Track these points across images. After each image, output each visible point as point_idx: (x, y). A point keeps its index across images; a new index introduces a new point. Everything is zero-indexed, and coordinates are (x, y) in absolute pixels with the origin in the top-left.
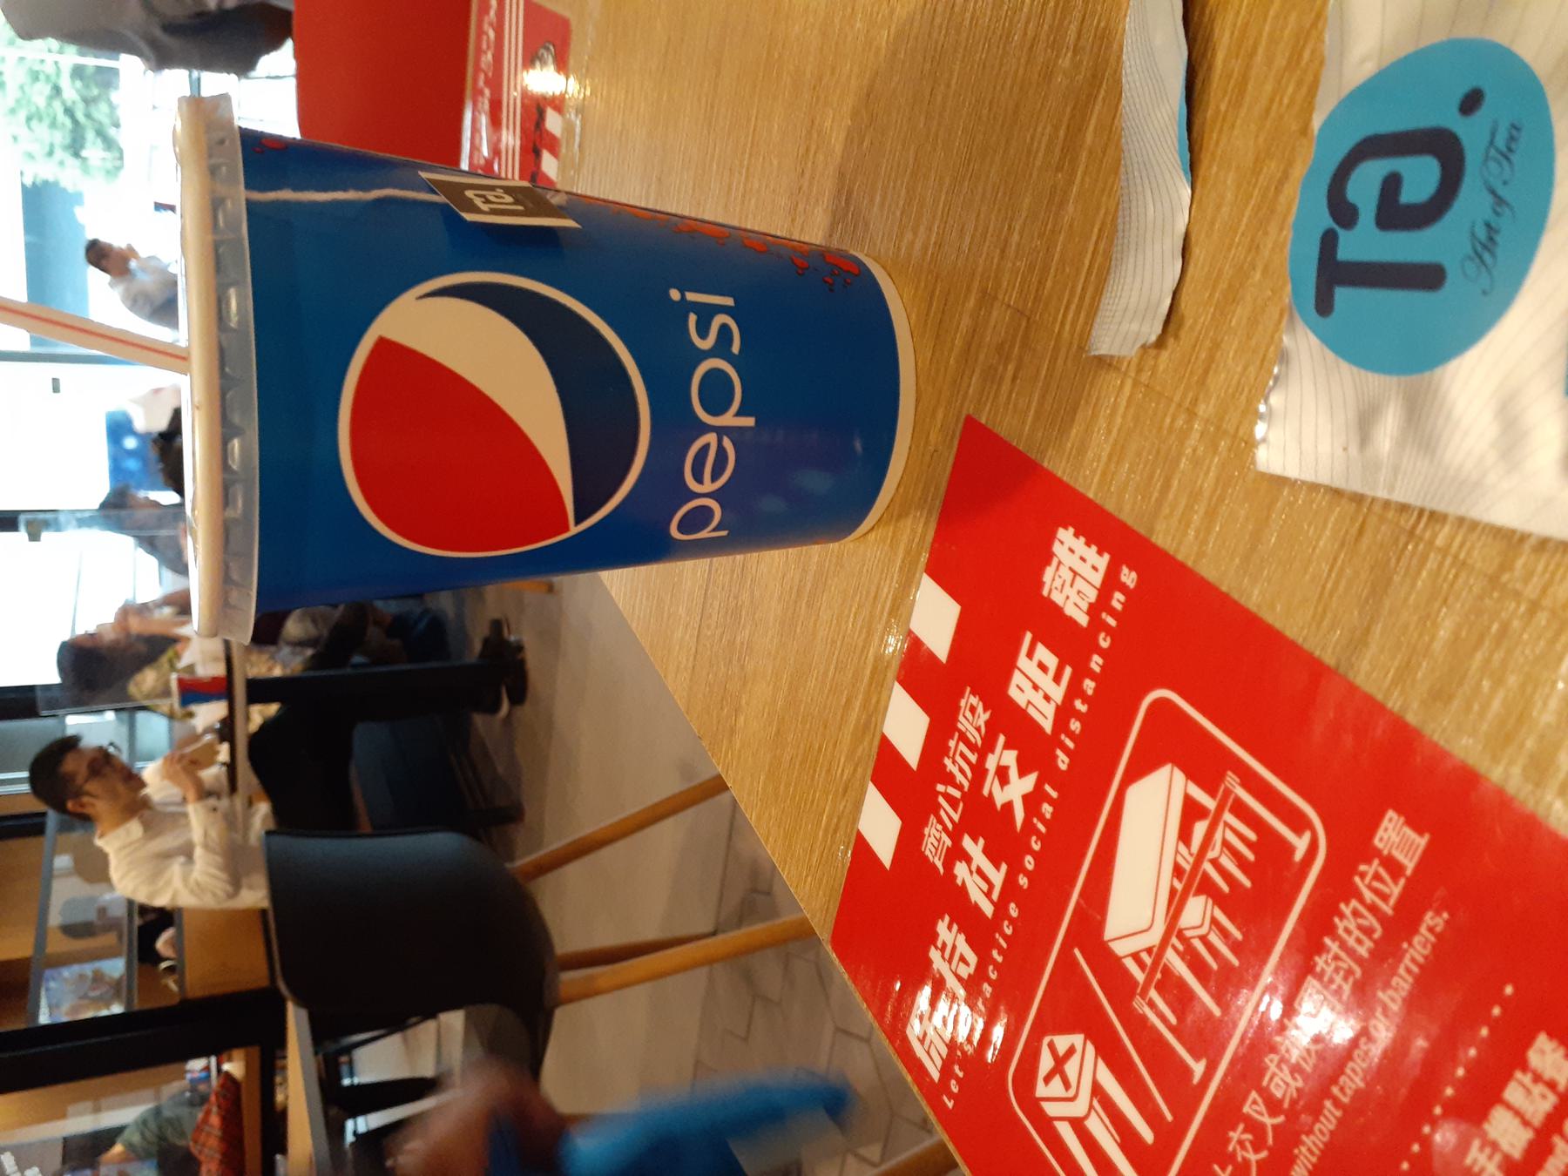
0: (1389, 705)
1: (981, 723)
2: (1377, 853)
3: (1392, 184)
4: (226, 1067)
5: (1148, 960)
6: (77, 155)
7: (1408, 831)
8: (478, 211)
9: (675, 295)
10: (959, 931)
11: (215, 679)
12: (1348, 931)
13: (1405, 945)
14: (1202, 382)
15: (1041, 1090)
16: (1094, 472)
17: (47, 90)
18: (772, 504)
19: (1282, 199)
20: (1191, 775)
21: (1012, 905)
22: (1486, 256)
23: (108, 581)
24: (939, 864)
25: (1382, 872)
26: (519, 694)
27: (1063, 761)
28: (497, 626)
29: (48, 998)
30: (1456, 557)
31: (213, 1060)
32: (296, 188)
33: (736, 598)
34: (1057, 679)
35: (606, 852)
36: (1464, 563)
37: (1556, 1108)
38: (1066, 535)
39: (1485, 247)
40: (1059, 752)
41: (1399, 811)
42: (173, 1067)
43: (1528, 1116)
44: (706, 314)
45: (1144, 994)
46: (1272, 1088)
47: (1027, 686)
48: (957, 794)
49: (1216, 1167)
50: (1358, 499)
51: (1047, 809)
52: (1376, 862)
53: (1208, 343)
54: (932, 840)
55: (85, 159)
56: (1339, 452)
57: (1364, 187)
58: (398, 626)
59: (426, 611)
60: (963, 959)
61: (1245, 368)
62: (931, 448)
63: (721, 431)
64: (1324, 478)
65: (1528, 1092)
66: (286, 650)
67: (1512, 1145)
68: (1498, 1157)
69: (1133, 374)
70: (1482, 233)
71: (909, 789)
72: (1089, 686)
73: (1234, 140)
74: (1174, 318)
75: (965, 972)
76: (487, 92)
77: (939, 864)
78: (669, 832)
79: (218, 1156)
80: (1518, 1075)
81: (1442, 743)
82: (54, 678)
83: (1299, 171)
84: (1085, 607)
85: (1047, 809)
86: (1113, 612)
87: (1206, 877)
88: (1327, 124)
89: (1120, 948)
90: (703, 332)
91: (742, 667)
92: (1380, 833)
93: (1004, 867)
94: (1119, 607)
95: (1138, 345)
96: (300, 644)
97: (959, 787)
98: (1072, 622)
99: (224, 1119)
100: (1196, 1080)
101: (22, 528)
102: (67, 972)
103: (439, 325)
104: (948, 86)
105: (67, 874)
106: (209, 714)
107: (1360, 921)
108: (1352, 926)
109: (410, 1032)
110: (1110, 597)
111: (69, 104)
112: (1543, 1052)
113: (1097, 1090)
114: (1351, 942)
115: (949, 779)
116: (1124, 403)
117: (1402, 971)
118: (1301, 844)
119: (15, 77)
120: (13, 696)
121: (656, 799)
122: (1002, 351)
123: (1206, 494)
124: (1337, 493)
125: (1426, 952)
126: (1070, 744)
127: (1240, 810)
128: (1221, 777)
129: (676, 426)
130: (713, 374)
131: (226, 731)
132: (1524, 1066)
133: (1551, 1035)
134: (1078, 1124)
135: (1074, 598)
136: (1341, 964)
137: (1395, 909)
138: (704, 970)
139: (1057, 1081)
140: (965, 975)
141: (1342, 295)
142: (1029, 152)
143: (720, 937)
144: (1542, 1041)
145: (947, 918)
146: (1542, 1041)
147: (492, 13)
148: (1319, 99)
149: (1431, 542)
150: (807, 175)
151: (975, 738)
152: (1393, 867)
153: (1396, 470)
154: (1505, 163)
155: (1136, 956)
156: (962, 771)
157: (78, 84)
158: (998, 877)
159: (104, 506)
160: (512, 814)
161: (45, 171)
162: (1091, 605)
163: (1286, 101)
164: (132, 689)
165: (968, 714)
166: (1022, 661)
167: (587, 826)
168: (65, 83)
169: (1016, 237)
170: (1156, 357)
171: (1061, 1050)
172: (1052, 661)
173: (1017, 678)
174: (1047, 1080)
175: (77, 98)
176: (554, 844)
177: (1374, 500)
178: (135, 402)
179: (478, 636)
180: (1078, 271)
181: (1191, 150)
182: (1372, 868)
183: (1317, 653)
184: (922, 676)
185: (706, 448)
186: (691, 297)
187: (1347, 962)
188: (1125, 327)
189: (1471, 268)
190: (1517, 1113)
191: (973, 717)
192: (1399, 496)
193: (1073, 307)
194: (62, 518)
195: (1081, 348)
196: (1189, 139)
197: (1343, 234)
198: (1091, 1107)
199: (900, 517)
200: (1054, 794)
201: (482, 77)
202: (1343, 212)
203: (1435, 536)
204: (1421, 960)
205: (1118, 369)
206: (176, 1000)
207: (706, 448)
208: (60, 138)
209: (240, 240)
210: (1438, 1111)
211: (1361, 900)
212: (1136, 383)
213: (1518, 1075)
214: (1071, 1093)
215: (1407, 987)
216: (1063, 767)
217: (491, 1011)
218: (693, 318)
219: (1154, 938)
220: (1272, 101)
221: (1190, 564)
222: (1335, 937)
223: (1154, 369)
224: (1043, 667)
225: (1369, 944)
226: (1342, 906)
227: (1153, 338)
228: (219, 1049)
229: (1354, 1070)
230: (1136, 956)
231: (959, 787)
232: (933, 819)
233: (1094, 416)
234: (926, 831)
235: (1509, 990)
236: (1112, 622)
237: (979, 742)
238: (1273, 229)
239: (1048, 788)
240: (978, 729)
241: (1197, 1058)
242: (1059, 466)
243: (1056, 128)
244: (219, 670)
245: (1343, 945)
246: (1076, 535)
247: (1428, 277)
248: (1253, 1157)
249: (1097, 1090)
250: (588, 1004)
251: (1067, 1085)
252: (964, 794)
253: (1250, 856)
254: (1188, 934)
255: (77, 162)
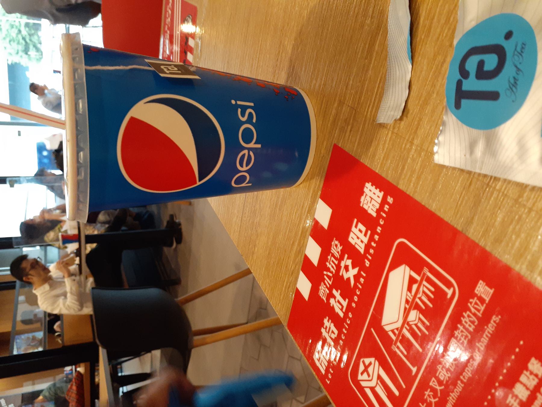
0: (480, 244)
1: (339, 250)
2: (476, 295)
3: (481, 64)
4: (78, 369)
5: (397, 332)
6: (26, 53)
7: (487, 288)
8: (165, 73)
9: (233, 102)
10: (332, 322)
11: (74, 235)
12: (466, 322)
13: (486, 327)
14: (416, 132)
15: (360, 377)
16: (378, 163)
17: (16, 31)
18: (267, 175)
19: (443, 69)
20: (412, 268)
21: (350, 313)
22: (514, 89)
23: (37, 201)
24: (325, 299)
25: (478, 302)
26: (179, 240)
27: (367, 263)
28: (172, 216)
29: (17, 345)
30: (503, 193)
31: (74, 367)
32: (102, 65)
33: (254, 207)
34: (365, 235)
35: (209, 295)
36: (506, 195)
37: (538, 383)
38: (368, 185)
39: (513, 85)
40: (366, 260)
41: (484, 281)
42: (60, 369)
43: (528, 386)
44: (244, 109)
45: (395, 344)
46: (440, 376)
47: (355, 237)
48: (331, 275)
49: (420, 404)
50: (469, 173)
51: (362, 280)
52: (476, 298)
53: (417, 119)
54: (322, 291)
55: (29, 55)
56: (463, 156)
57: (472, 65)
58: (138, 217)
59: (147, 211)
60: (333, 332)
61: (430, 127)
62: (322, 155)
63: (249, 149)
64: (458, 165)
65: (528, 378)
66: (99, 225)
67: (523, 396)
68: (518, 401)
69: (391, 129)
70: (512, 81)
71: (314, 273)
72: (376, 237)
73: (427, 48)
74: (406, 110)
75: (334, 336)
76: (168, 32)
77: (325, 299)
78: (231, 288)
79: (75, 400)
80: (525, 372)
81: (498, 257)
82: (18, 234)
83: (449, 59)
84: (375, 210)
85: (362, 280)
86: (385, 212)
87: (417, 304)
88: (459, 43)
89: (387, 328)
90: (243, 115)
91: (257, 231)
92: (477, 288)
93: (347, 300)
94: (387, 210)
95: (393, 119)
96: (104, 223)
97: (332, 272)
98: (370, 215)
99: (77, 387)
100: (413, 374)
101: (8, 183)
102: (23, 337)
103: (152, 112)
104: (328, 30)
105: (23, 302)
106: (72, 247)
107: (470, 319)
108: (467, 321)
109: (142, 357)
110: (384, 207)
111: (24, 36)
112: (533, 364)
113: (379, 377)
114: (467, 326)
115: (328, 270)
116: (389, 139)
117: (484, 336)
118: (450, 292)
119: (5, 27)
120: (4, 241)
121: (227, 277)
122: (346, 121)
123: (417, 171)
124: (462, 171)
125: (493, 329)
126: (370, 258)
127: (429, 280)
128: (422, 269)
129: (234, 148)
130: (247, 129)
131: (78, 253)
132: (527, 369)
133: (536, 358)
134: (373, 389)
135: (371, 207)
136: (463, 334)
137: (482, 314)
138: (243, 336)
139: (365, 374)
140: (333, 337)
141: (464, 102)
142: (356, 52)
143: (249, 324)
144: (533, 360)
145: (327, 318)
146: (533, 360)
147: (170, 5)
148: (456, 34)
149: (495, 188)
150: (279, 61)
151: (337, 255)
152: (482, 300)
153: (482, 163)
154: (520, 56)
155: (393, 331)
156: (332, 267)
157: (27, 29)
158: (345, 303)
159: (36, 175)
160: (177, 282)
161: (15, 59)
162: (377, 209)
163: (444, 35)
164: (46, 238)
165: (335, 247)
166: (353, 229)
167: (203, 286)
168: (23, 29)
169: (351, 82)
170: (400, 124)
171: (367, 363)
172: (363, 229)
173: (352, 235)
174: (362, 374)
175: (27, 34)
176: (191, 292)
177: (475, 173)
178: (47, 139)
179: (165, 220)
180: (373, 94)
181: (412, 52)
182: (474, 300)
183: (455, 226)
184: (319, 234)
185: (244, 155)
186: (239, 103)
187: (466, 333)
188: (389, 113)
189: (508, 93)
190: (525, 385)
191: (336, 248)
192: (483, 172)
193: (371, 106)
194: (21, 179)
195: (374, 121)
196: (411, 48)
197: (464, 81)
198: (377, 383)
199: (311, 179)
200: (364, 275)
201: (167, 27)
202: (464, 74)
203: (496, 185)
204: (491, 332)
205: (386, 128)
206: (61, 346)
207: (244, 155)
208: (21, 48)
209: (83, 83)
210: (497, 384)
211: (471, 311)
212: (393, 133)
213: (525, 372)
214: (370, 378)
215: (486, 341)
216: (368, 265)
217: (170, 350)
218: (239, 110)
219: (399, 325)
220: (440, 35)
221: (411, 195)
222: (462, 324)
223: (399, 128)
224: (360, 231)
225: (473, 327)
226: (464, 314)
227: (399, 117)
228: (76, 363)
229: (468, 370)
230: (393, 331)
231: (332, 272)
232: (322, 284)
233: (378, 144)
234: (320, 288)
235: (522, 343)
236: (384, 215)
237: (339, 257)
238: (440, 79)
239: (362, 273)
240: (338, 252)
241: (414, 366)
242: (366, 161)
243: (365, 44)
244: (76, 232)
245: (464, 327)
246: (372, 185)
247: (493, 96)
248: (433, 401)
249: (379, 377)
250: (203, 348)
251: (369, 375)
252: (333, 275)
253: (432, 296)
254: (411, 323)
255: (27, 56)
